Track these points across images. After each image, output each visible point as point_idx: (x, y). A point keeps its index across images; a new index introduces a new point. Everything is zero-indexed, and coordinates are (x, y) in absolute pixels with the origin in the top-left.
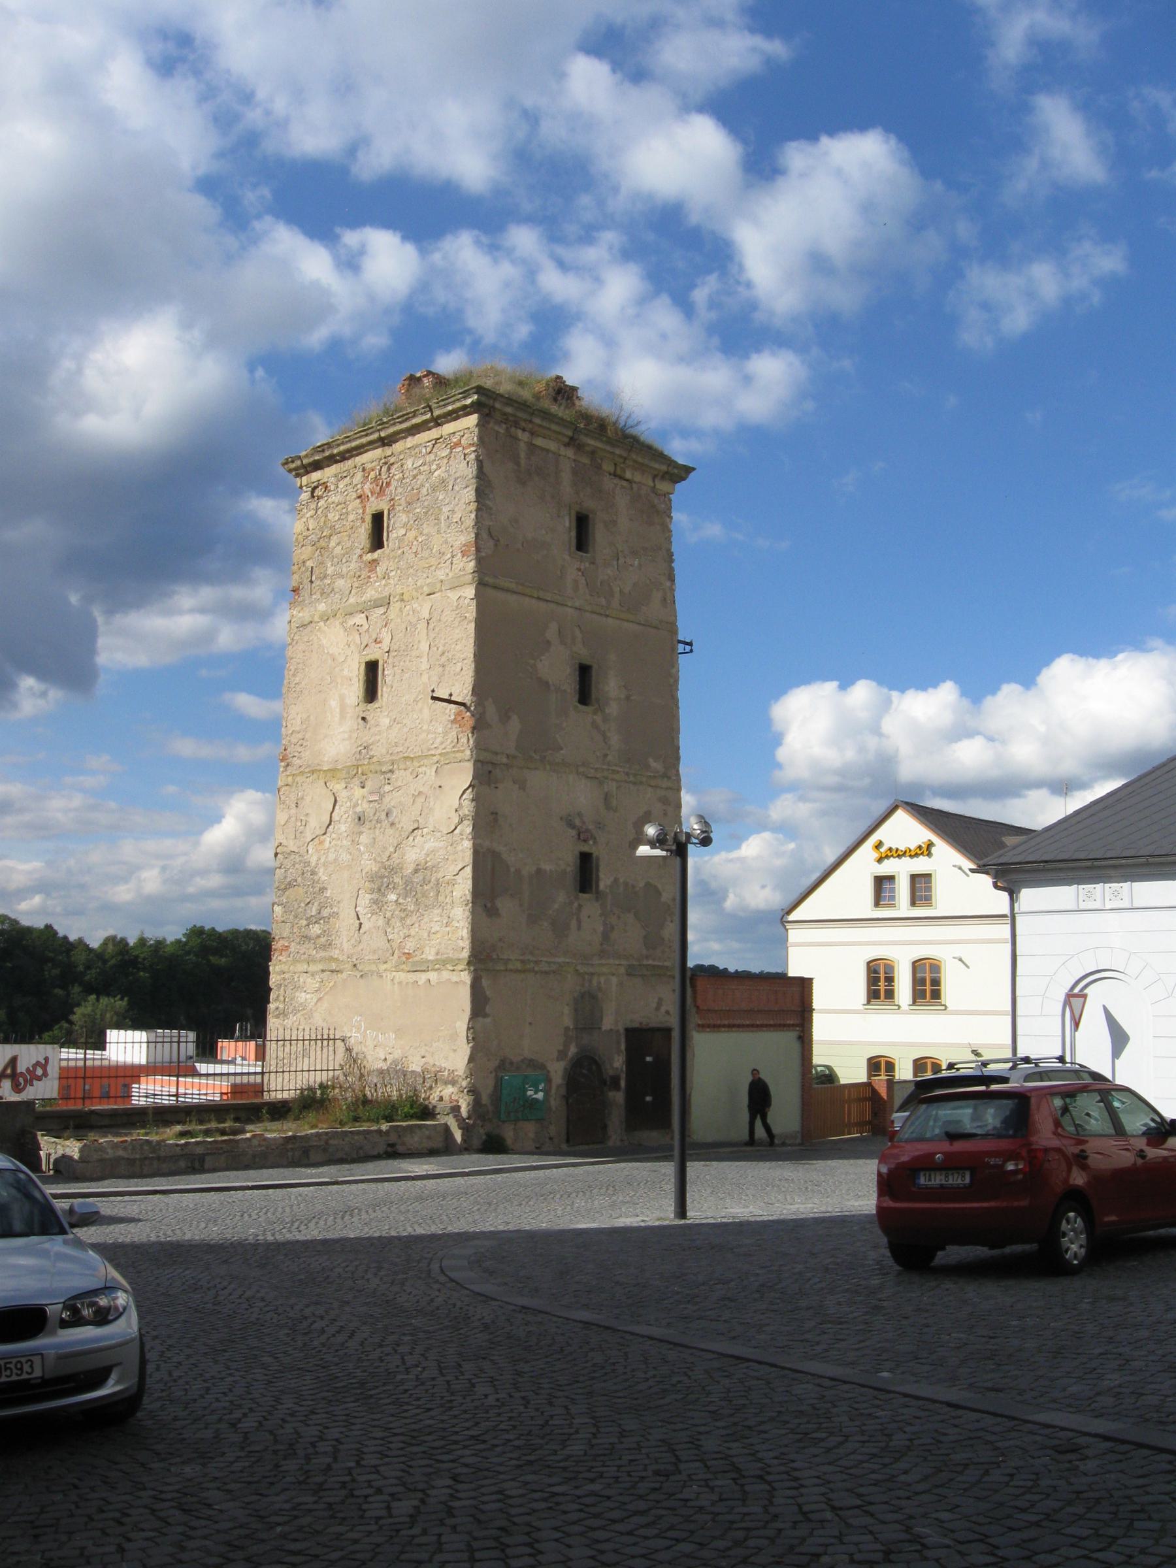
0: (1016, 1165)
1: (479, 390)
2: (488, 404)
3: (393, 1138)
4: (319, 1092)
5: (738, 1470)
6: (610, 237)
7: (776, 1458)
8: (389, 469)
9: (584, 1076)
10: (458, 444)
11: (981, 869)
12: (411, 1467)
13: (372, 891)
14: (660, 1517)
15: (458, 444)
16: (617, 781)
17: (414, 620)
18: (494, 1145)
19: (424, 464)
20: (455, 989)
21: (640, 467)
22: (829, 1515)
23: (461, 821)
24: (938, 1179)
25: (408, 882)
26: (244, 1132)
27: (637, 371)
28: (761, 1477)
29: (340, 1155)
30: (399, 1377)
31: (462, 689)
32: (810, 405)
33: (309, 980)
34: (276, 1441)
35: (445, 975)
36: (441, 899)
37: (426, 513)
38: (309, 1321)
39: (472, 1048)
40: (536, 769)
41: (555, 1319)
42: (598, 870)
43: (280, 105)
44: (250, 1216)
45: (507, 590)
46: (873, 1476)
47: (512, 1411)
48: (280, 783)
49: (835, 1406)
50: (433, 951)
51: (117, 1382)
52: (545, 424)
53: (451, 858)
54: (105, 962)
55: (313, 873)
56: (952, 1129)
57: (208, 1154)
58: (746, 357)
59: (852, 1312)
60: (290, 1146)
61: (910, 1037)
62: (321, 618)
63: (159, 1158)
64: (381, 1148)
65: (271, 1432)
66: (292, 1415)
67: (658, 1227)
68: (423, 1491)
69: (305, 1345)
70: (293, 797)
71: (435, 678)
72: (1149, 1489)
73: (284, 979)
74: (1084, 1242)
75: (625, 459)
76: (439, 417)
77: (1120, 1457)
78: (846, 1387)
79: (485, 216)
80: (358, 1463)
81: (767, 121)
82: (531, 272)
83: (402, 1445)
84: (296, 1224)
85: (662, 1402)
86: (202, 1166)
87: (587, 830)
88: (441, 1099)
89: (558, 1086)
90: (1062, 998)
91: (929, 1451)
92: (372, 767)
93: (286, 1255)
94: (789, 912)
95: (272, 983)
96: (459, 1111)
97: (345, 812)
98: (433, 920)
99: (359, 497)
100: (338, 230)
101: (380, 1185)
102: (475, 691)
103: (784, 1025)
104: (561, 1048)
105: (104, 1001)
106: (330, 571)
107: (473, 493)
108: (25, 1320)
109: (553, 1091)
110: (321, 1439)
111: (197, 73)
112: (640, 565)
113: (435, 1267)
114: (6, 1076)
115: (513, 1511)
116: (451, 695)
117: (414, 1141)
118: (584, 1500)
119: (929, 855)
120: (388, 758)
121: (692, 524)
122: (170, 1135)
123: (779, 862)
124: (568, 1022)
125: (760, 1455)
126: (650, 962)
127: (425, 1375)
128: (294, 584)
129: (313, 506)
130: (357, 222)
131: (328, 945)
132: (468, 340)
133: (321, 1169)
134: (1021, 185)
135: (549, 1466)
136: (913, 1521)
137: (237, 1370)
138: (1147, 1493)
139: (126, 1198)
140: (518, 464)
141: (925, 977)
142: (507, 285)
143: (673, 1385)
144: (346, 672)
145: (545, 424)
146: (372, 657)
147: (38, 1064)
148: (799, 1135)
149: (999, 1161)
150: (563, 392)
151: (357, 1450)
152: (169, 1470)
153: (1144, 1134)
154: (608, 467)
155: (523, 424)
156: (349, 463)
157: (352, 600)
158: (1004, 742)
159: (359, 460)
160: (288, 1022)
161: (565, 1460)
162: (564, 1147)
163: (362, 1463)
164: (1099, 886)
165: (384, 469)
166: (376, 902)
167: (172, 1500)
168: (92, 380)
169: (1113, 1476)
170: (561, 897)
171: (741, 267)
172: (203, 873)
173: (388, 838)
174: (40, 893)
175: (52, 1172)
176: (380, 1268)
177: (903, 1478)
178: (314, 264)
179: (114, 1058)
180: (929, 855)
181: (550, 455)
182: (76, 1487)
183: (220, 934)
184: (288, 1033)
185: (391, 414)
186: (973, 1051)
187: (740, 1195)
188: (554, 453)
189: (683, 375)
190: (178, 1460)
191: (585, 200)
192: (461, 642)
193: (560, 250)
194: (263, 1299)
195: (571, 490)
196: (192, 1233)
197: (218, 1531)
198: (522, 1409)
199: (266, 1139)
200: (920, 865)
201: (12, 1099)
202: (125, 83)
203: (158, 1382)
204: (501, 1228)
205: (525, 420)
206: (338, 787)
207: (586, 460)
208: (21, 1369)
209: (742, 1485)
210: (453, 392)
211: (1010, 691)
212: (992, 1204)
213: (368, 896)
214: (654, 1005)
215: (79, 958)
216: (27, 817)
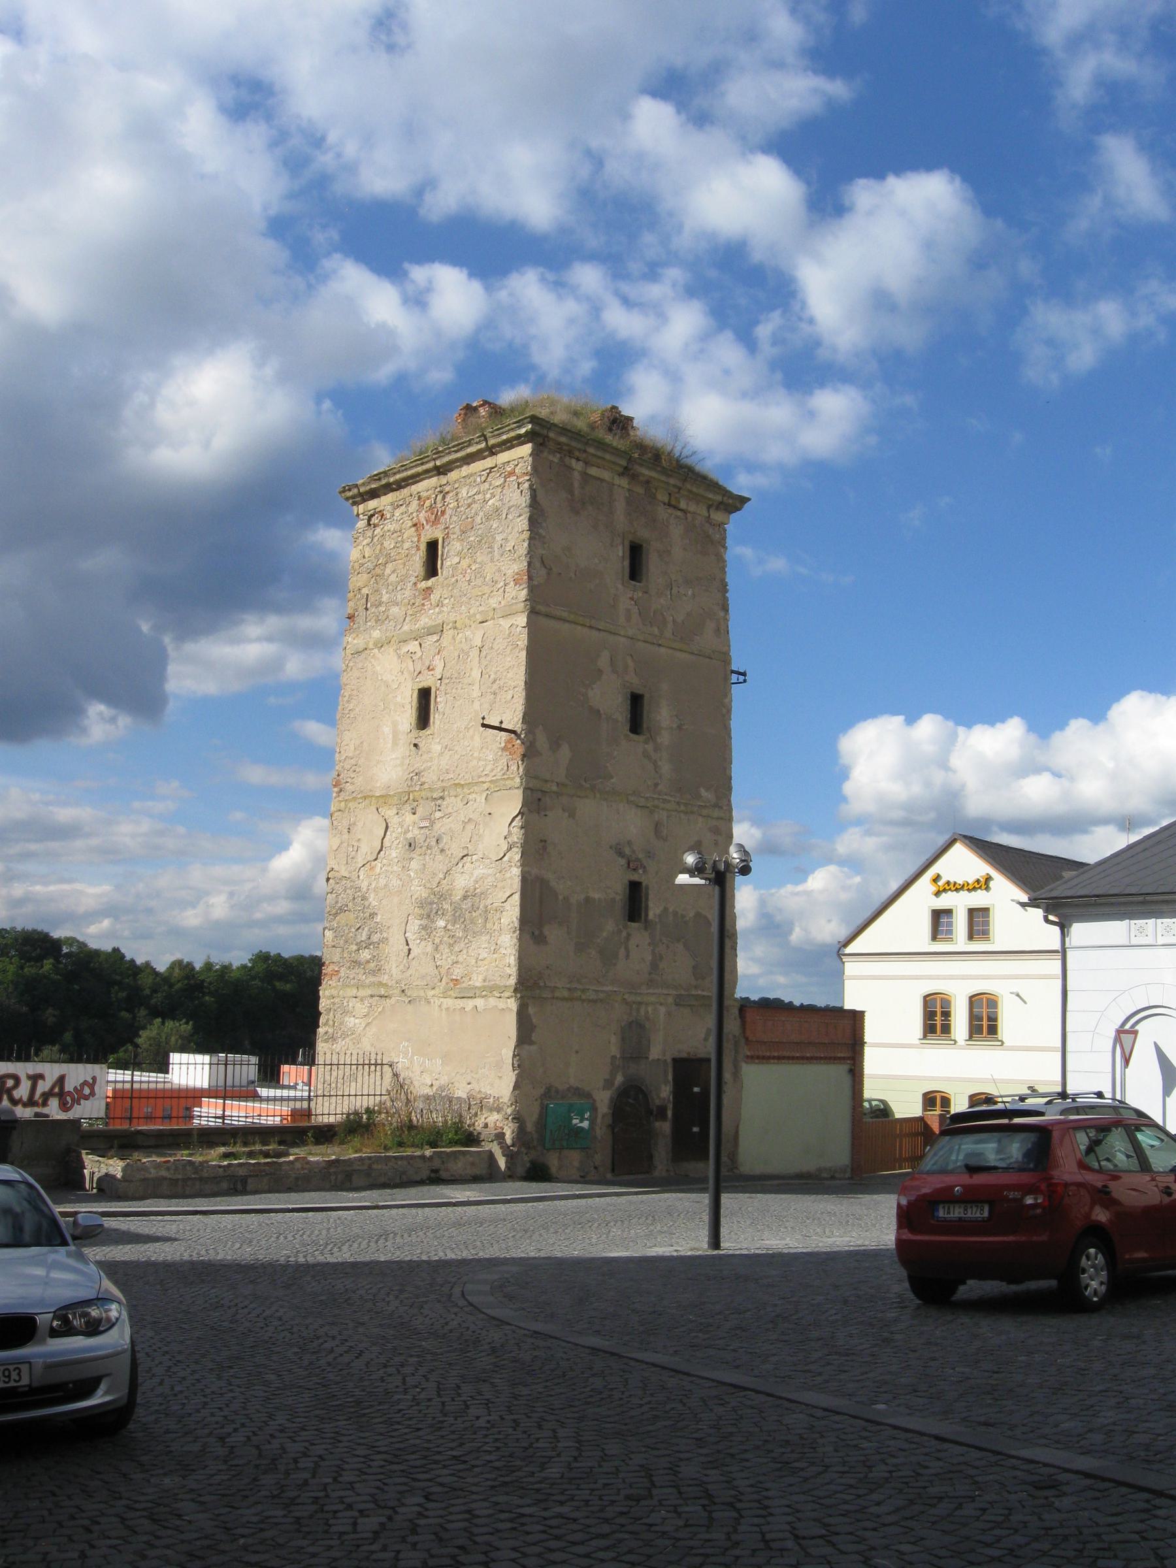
0: (1036, 1199)
1: (534, 419)
2: (543, 434)
3: (437, 1164)
4: (365, 1117)
5: (710, 1496)
6: (674, 274)
7: (752, 1486)
8: (444, 498)
9: (631, 1105)
10: (512, 473)
11: (1033, 903)
12: (385, 1484)
13: (421, 917)
14: (620, 1541)
15: (512, 473)
17: (466, 648)
18: (538, 1173)
19: (478, 493)
20: (501, 1016)
21: (696, 498)
22: (790, 1544)
24: (957, 1212)
25: (456, 908)
26: (287, 1154)
27: (699, 405)
28: (731, 1504)
29: (382, 1180)
30: (397, 1397)
31: (513, 717)
32: (872, 440)
33: (358, 1005)
34: (260, 1455)
35: (492, 1001)
36: (489, 926)
37: (480, 541)
38: (321, 1341)
40: (587, 797)
41: (564, 1344)
42: (647, 899)
43: (351, 149)
44: (286, 1238)
46: (846, 1507)
47: (499, 1433)
48: (333, 809)
49: (822, 1437)
50: (481, 978)
51: (106, 1393)
52: (599, 454)
54: (171, 986)
55: (364, 898)
56: (973, 1162)
58: (811, 393)
59: (861, 1344)
61: (966, 1072)
62: (375, 645)
63: (201, 1179)
64: (425, 1174)
65: (257, 1447)
66: (281, 1431)
67: (689, 1257)
68: (393, 1508)
69: (311, 1363)
70: (345, 823)
71: (486, 706)
72: (1118, 1527)
73: (334, 1004)
74: (1105, 1279)
75: (680, 489)
76: (494, 446)
77: (1098, 1494)
78: (837, 1418)
79: (549, 254)
80: (335, 1479)
81: (829, 161)
82: (596, 310)
83: (383, 1463)
84: (329, 1248)
85: (650, 1428)
86: (245, 1187)
87: (637, 860)
88: (486, 1126)
90: (1113, 1034)
91: (907, 1483)
92: (423, 794)
93: (313, 1277)
94: (846, 945)
97: (397, 838)
98: (481, 947)
99: (415, 525)
100: (406, 265)
101: (420, 1211)
103: (835, 1058)
104: (607, 1077)
105: (170, 1024)
106: (385, 598)
107: (526, 522)
108: (13, 1329)
109: (599, 1120)
110: (305, 1455)
111: (269, 117)
112: (694, 595)
113: (457, 1291)
115: (476, 1530)
117: (458, 1167)
118: (548, 1522)
119: (987, 889)
121: (748, 556)
122: (213, 1156)
123: (844, 896)
124: (615, 1050)
125: (735, 1483)
127: (422, 1396)
128: (350, 611)
129: (369, 534)
132: (532, 377)
133: (363, 1194)
134: (1083, 224)
135: (523, 1488)
136: (873, 1553)
137: (239, 1387)
138: (1118, 1531)
139: (166, 1218)
140: (571, 493)
141: (979, 1011)
142: (571, 321)
143: (666, 1412)
144: (399, 699)
145: (599, 454)
146: (425, 684)
147: (85, 1083)
148: (849, 1170)
149: (1017, 1195)
150: (619, 423)
151: (338, 1466)
152: (149, 1481)
154: (662, 496)
155: (577, 453)
156: (405, 492)
157: (406, 628)
158: (1072, 779)
159: (415, 488)
160: (337, 1047)
161: (540, 1482)
162: (609, 1176)
163: (340, 1479)
164: (1151, 922)
165: (440, 497)
166: (425, 928)
167: (144, 1510)
168: (164, 415)
169: (1086, 1513)
170: (610, 926)
171: (804, 305)
172: (272, 898)
173: (438, 864)
174: (107, 916)
175: (95, 1191)
176: (401, 1291)
177: (875, 1509)
178: (379, 303)
179: (176, 1081)
180: (987, 889)
182: (54, 1494)
183: (286, 960)
184: (335, 1057)
185: (447, 443)
186: (1029, 1088)
187: (768, 1228)
189: (748, 410)
190: (161, 1471)
192: (513, 670)
193: (625, 287)
194: (280, 1319)
195: (624, 521)
196: (226, 1253)
197: (183, 1542)
198: (510, 1431)
199: (308, 1162)
200: (978, 899)
201: (59, 1117)
202: (200, 127)
203: (157, 1396)
204: (532, 1254)
205: (579, 450)
206: (390, 813)
207: (640, 490)
208: (9, 1376)
209: (710, 1512)
210: (508, 421)
211: (1078, 725)
212: (1011, 1238)
213: (418, 922)
215: (146, 981)
216: (94, 842)
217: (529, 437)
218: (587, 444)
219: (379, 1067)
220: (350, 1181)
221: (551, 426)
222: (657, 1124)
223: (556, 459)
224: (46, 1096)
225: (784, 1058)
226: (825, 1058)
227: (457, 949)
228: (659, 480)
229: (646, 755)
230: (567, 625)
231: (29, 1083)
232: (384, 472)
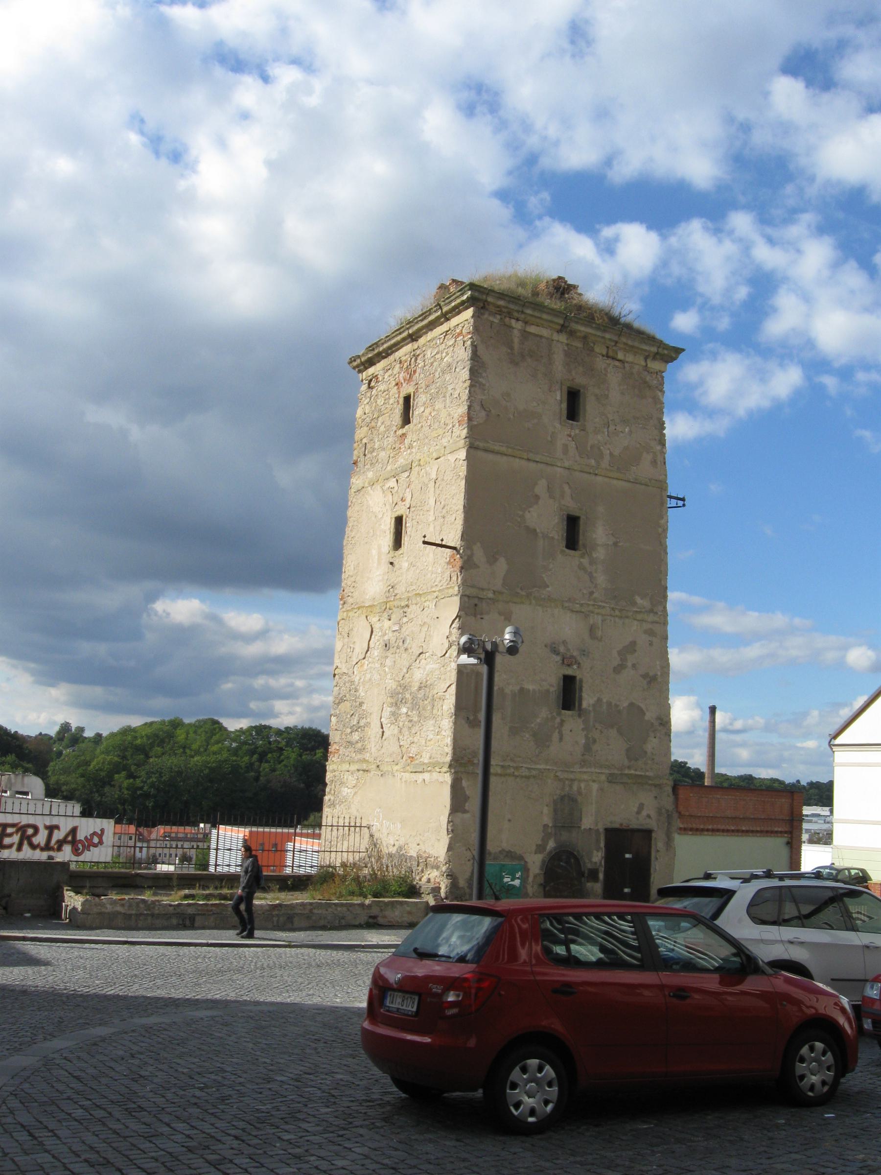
1: (472, 286)
3: (375, 911)
8: (416, 359)
13: (392, 705)
15: (460, 334)
16: (603, 615)
17: (426, 481)
19: (437, 353)
21: (632, 349)
23: (450, 646)
29: (322, 923)
33: (350, 777)
36: (435, 711)
39: (451, 838)
40: (522, 603)
45: (498, 453)
52: (537, 314)
53: (443, 677)
57: (199, 914)
60: (274, 913)
63: (153, 915)
64: (363, 919)
75: (616, 342)
76: (447, 313)
79: (712, 207)
82: (746, 247)
87: (572, 657)
88: (429, 881)
89: (535, 876)
92: (396, 603)
94: (835, 737)
95: (327, 781)
96: (439, 892)
97: (378, 640)
100: (598, 226)
102: (463, 537)
103: (772, 832)
104: (540, 842)
107: (468, 373)
109: (531, 879)
112: (631, 432)
114: (68, 842)
116: (442, 540)
117: (395, 915)
120: (406, 595)
124: (547, 820)
126: (632, 772)
130: (612, 220)
131: (362, 750)
140: (512, 348)
144: (382, 527)
146: (398, 513)
147: (95, 833)
153: (717, 970)
154: (600, 349)
155: (516, 314)
156: (391, 358)
165: (413, 360)
173: (404, 660)
181: (543, 340)
184: (335, 820)
188: (547, 339)
191: (789, 189)
193: (769, 230)
205: (518, 311)
207: (578, 344)
213: (389, 709)
214: (635, 809)
217: (472, 302)
218: (524, 306)
219: (358, 829)
220: (292, 923)
221: (489, 291)
222: (589, 885)
223: (496, 320)
224: (61, 844)
225: (718, 830)
226: (761, 832)
227: (413, 731)
228: (595, 335)
229: (581, 567)
230: (505, 458)
231: (46, 832)
232: (376, 343)
